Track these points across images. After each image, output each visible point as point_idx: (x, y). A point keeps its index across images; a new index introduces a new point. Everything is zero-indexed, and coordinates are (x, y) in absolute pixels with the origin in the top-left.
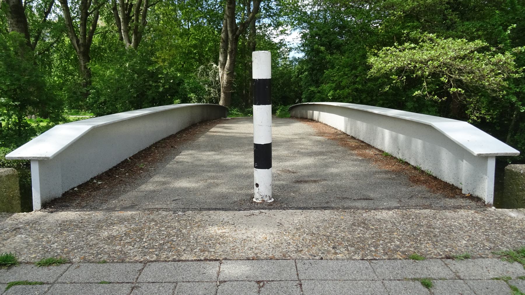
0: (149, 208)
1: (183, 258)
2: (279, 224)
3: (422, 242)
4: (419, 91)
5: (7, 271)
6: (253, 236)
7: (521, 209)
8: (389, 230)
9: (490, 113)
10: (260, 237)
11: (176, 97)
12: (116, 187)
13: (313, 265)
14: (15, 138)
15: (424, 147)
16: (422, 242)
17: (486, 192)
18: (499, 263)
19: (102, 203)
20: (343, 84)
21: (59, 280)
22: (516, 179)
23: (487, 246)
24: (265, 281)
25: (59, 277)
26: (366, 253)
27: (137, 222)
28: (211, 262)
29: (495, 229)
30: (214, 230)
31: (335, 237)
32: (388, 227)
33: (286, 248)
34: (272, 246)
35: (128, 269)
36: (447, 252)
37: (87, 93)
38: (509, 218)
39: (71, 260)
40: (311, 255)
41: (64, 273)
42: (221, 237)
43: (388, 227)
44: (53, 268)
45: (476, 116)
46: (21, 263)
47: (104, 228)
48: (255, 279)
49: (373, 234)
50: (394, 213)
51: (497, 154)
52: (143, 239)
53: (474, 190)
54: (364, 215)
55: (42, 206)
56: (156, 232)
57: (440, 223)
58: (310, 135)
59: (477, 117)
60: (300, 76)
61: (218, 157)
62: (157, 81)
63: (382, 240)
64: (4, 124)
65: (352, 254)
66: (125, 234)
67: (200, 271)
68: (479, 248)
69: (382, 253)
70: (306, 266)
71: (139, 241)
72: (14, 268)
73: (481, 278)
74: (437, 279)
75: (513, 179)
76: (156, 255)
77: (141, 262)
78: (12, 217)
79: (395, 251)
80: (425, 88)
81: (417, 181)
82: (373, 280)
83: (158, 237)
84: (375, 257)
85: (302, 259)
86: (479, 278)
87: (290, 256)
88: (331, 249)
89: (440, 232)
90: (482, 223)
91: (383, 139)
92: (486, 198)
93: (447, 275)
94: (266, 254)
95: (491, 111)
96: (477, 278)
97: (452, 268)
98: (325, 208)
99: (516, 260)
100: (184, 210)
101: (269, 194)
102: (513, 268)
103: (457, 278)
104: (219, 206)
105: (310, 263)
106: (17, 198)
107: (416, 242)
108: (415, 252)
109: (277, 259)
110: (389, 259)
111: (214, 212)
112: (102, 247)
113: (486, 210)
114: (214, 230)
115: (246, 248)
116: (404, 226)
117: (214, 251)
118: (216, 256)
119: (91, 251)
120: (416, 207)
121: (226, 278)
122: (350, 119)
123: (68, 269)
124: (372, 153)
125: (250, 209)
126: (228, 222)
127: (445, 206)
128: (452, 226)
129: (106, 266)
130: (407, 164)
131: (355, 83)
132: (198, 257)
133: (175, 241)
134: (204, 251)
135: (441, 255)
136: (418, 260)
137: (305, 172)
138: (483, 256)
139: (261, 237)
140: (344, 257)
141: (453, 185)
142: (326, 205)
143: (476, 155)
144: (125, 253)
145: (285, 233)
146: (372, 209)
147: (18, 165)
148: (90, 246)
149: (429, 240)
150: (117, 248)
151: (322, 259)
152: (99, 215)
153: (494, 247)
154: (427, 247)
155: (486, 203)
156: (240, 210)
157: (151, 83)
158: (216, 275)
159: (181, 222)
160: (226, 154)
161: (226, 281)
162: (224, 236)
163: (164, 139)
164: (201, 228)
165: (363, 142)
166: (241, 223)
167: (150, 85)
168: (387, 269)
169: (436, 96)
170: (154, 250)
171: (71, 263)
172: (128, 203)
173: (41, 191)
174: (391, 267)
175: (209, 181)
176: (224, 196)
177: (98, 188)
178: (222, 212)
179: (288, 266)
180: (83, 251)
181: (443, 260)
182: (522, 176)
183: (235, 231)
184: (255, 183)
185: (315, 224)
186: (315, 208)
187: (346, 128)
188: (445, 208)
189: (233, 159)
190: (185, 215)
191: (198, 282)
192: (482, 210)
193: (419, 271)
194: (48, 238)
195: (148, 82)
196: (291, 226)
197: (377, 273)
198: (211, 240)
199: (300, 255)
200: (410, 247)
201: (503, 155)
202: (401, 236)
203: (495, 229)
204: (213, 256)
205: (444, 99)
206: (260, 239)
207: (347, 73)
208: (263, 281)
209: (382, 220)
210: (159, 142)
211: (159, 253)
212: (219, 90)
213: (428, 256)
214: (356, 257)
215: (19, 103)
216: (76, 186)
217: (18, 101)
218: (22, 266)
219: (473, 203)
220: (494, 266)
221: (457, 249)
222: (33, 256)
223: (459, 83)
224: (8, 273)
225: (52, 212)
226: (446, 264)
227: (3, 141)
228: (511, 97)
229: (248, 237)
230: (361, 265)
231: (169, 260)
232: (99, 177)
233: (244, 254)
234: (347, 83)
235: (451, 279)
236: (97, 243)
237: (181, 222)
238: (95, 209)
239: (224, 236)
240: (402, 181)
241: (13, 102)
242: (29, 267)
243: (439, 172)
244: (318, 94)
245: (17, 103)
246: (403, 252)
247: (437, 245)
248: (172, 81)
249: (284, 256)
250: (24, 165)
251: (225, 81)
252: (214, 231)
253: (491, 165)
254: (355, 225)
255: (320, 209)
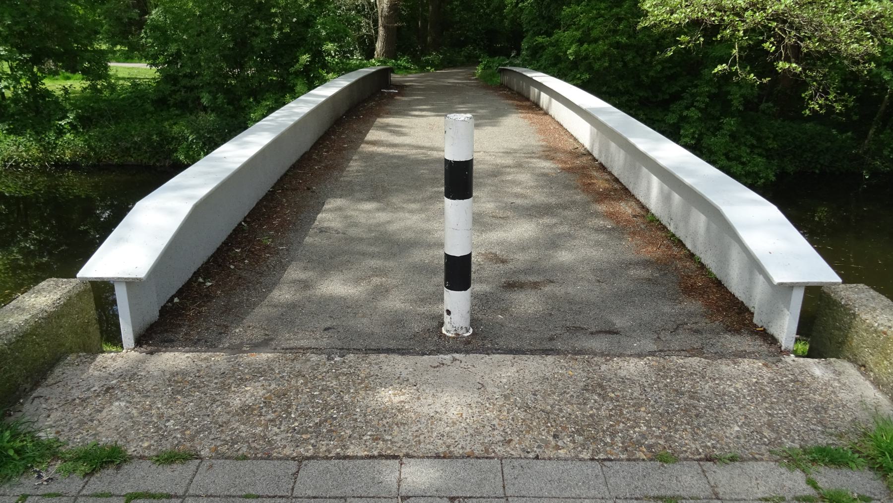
0: (292, 345)
1: (349, 452)
2: (480, 386)
3: (677, 427)
4: (724, 65)
5: (117, 473)
6: (443, 410)
7: (832, 360)
8: (635, 401)
9: (843, 97)
10: (453, 412)
11: (302, 48)
12: (234, 294)
13: (525, 470)
14: (30, 118)
15: (708, 230)
16: (677, 427)
17: (785, 334)
18: (775, 471)
19: (221, 333)
20: (595, 33)
21: (191, 492)
22: (834, 310)
23: (766, 437)
24: (461, 497)
25: (189, 484)
26: (598, 448)
27: (278, 376)
28: (388, 462)
29: (786, 401)
30: (388, 396)
31: (558, 415)
32: (635, 394)
33: (490, 436)
34: (471, 431)
35: (279, 472)
36: (709, 448)
37: (141, 20)
38: (809, 379)
39: (199, 453)
40: (523, 450)
41: (193, 478)
42: (399, 411)
43: (635, 394)
44: (178, 467)
45: (818, 103)
46: (131, 458)
47: (233, 389)
48: (448, 494)
49: (611, 410)
50: (646, 364)
51: (808, 283)
52: (290, 413)
53: (769, 324)
54: (603, 367)
55: (135, 343)
56: (307, 400)
57: (710, 387)
58: (532, 154)
59: (820, 106)
60: (520, 5)
61: (383, 217)
62: (268, 18)
63: (623, 423)
64: (8, 94)
65: (580, 448)
66: (264, 402)
67: (374, 478)
68: (753, 441)
69: (620, 449)
70: (516, 472)
71: (286, 418)
72: (126, 467)
73: (745, 498)
74: (687, 497)
75: (830, 309)
76: (313, 446)
77: (293, 459)
78: (95, 363)
79: (639, 444)
80: (735, 56)
81: (689, 290)
82: (602, 498)
83: (311, 410)
84: (609, 456)
85: (512, 457)
86: (744, 497)
87: (494, 452)
88: (551, 438)
89: (706, 407)
90: (768, 389)
91: (649, 189)
92: (783, 342)
93: (702, 491)
94: (462, 448)
95: (847, 94)
96: (740, 497)
97: (710, 479)
98: (546, 352)
99: (798, 467)
100: (344, 351)
101: (466, 323)
102: (791, 480)
103: (714, 497)
104: (393, 344)
105: (522, 467)
106: (94, 321)
107: (670, 428)
108: (665, 448)
109: (477, 458)
110: (628, 460)
111: (386, 357)
112: (237, 428)
113: (780, 361)
114: (388, 396)
115: (435, 434)
116: (657, 392)
117: (391, 440)
118: (395, 448)
119: (223, 437)
120: (680, 352)
121: (409, 491)
122: (599, 134)
123: (197, 469)
124: (630, 211)
125: (438, 352)
126: (408, 380)
127: (722, 352)
128: (724, 395)
129: (248, 463)
130: (680, 244)
131: (615, 32)
132: (368, 451)
133: (335, 418)
134: (376, 439)
135: (700, 454)
136: (667, 463)
137: (521, 259)
138: (757, 456)
139: (455, 413)
140: (568, 456)
141: (742, 302)
142: (548, 346)
143: (775, 284)
144: (269, 441)
145: (488, 405)
146: (615, 356)
147: (41, 166)
148: (220, 426)
149: (688, 425)
150: (257, 431)
151: (537, 458)
152: (219, 359)
153: (775, 439)
154: (684, 439)
155: (783, 349)
156: (423, 354)
157: (258, 23)
158: (396, 486)
159: (340, 377)
160: (396, 209)
161: (410, 497)
162: (404, 409)
163: (294, 167)
164: (370, 393)
165: (617, 180)
166: (426, 382)
167: (257, 28)
168: (624, 478)
169: (752, 75)
170: (309, 436)
171: (198, 457)
172: (258, 335)
173: (132, 322)
174: (629, 475)
175: (376, 280)
176: (397, 320)
177: (208, 297)
178: (398, 358)
179: (491, 471)
180: (212, 437)
181: (701, 463)
182: (842, 309)
183: (419, 398)
184: (445, 309)
185: (530, 387)
186: (533, 352)
187: (592, 145)
188: (721, 356)
189: (409, 223)
190: (344, 362)
191: (373, 497)
192: (775, 361)
193: (665, 483)
194: (158, 408)
195: (252, 21)
196: (496, 390)
197: (609, 486)
198: (385, 418)
199: (508, 449)
200: (660, 437)
201: (816, 285)
202: (649, 415)
203: (786, 401)
204: (390, 449)
205: (765, 81)
206: (454, 417)
207: (604, 14)
208: (458, 497)
209: (628, 379)
210: (285, 175)
211: (317, 442)
212: (376, 22)
213: (682, 455)
214: (585, 455)
215: (30, 56)
216: (174, 292)
217: (28, 53)
218: (135, 462)
219: (765, 348)
220: (768, 477)
221: (723, 443)
222: (146, 444)
223: (796, 53)
224: (119, 476)
225: (151, 353)
226: (703, 471)
227: (11, 124)
228: (884, 72)
229: (437, 412)
230: (589, 471)
231: (331, 455)
232: (205, 271)
233: (432, 447)
234: (602, 33)
235: (706, 498)
236: (229, 421)
237: (340, 377)
238: (212, 347)
239: (404, 409)
240: (667, 290)
241: (20, 55)
242: (145, 464)
243: (726, 276)
244: (551, 48)
245: (26, 56)
246: (649, 447)
247: (697, 434)
248: (295, 20)
249: (487, 451)
250: (52, 165)
251: (385, 6)
252: (387, 399)
253: (797, 298)
254: (587, 390)
255: (540, 354)
